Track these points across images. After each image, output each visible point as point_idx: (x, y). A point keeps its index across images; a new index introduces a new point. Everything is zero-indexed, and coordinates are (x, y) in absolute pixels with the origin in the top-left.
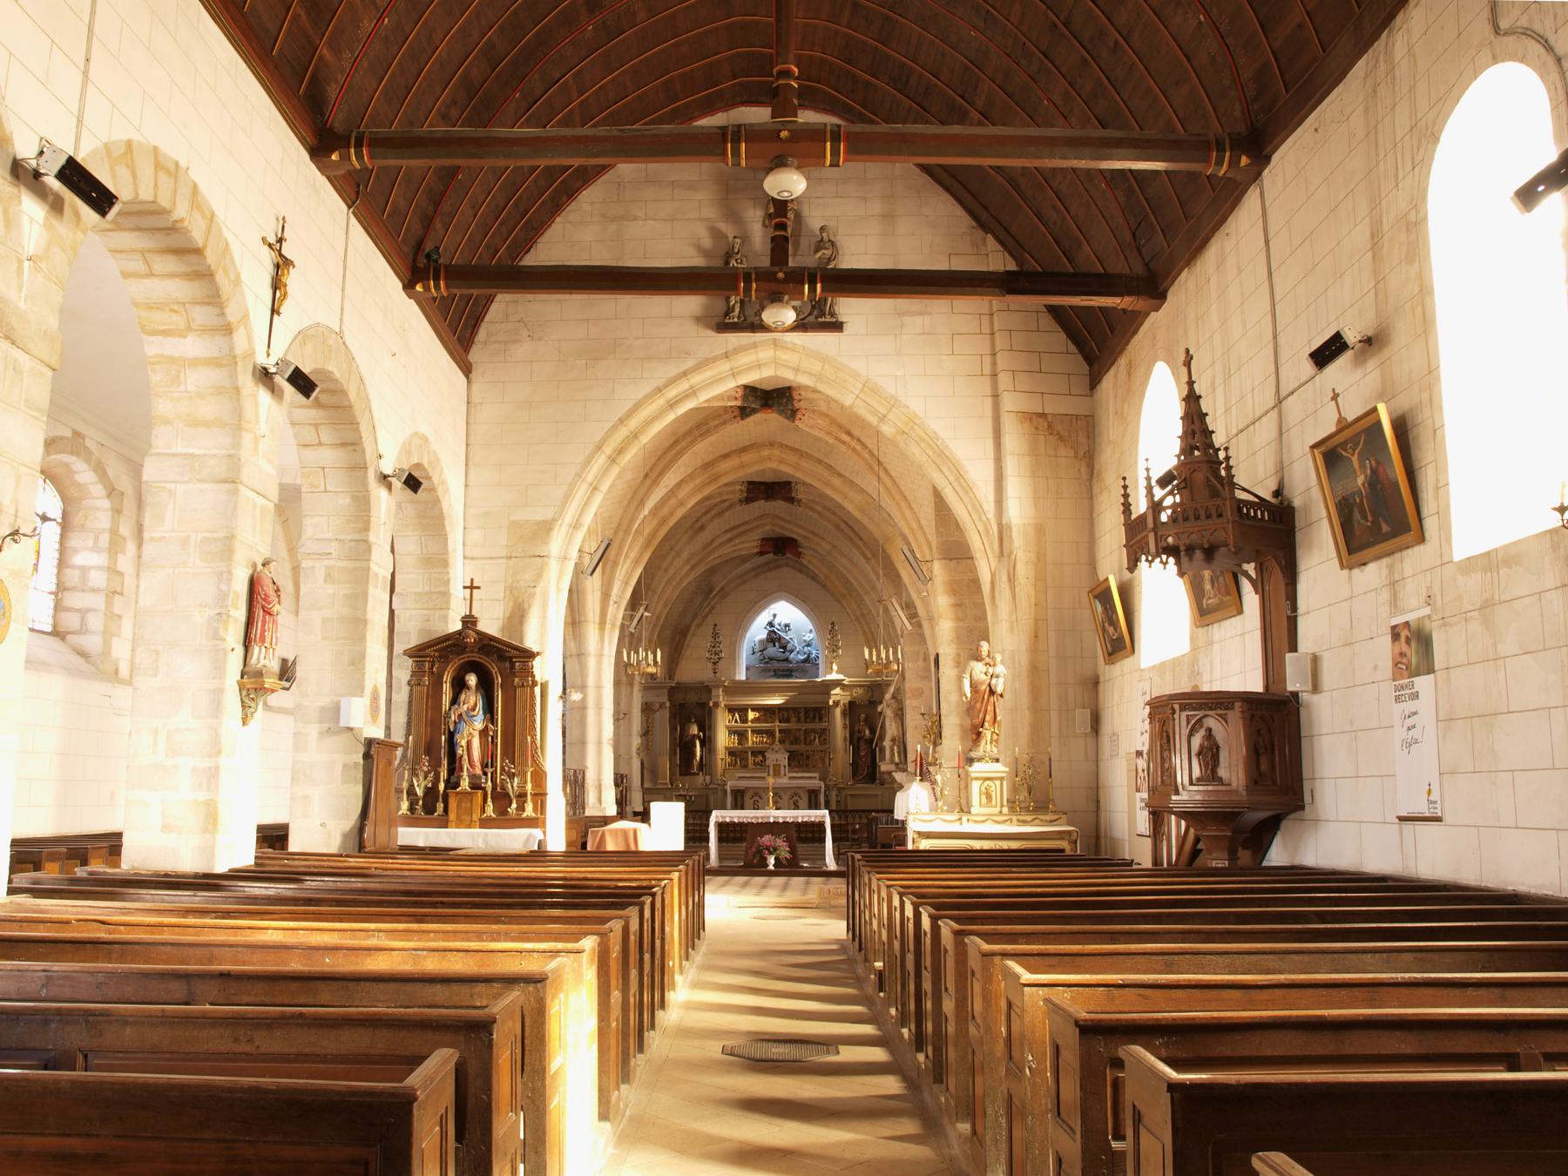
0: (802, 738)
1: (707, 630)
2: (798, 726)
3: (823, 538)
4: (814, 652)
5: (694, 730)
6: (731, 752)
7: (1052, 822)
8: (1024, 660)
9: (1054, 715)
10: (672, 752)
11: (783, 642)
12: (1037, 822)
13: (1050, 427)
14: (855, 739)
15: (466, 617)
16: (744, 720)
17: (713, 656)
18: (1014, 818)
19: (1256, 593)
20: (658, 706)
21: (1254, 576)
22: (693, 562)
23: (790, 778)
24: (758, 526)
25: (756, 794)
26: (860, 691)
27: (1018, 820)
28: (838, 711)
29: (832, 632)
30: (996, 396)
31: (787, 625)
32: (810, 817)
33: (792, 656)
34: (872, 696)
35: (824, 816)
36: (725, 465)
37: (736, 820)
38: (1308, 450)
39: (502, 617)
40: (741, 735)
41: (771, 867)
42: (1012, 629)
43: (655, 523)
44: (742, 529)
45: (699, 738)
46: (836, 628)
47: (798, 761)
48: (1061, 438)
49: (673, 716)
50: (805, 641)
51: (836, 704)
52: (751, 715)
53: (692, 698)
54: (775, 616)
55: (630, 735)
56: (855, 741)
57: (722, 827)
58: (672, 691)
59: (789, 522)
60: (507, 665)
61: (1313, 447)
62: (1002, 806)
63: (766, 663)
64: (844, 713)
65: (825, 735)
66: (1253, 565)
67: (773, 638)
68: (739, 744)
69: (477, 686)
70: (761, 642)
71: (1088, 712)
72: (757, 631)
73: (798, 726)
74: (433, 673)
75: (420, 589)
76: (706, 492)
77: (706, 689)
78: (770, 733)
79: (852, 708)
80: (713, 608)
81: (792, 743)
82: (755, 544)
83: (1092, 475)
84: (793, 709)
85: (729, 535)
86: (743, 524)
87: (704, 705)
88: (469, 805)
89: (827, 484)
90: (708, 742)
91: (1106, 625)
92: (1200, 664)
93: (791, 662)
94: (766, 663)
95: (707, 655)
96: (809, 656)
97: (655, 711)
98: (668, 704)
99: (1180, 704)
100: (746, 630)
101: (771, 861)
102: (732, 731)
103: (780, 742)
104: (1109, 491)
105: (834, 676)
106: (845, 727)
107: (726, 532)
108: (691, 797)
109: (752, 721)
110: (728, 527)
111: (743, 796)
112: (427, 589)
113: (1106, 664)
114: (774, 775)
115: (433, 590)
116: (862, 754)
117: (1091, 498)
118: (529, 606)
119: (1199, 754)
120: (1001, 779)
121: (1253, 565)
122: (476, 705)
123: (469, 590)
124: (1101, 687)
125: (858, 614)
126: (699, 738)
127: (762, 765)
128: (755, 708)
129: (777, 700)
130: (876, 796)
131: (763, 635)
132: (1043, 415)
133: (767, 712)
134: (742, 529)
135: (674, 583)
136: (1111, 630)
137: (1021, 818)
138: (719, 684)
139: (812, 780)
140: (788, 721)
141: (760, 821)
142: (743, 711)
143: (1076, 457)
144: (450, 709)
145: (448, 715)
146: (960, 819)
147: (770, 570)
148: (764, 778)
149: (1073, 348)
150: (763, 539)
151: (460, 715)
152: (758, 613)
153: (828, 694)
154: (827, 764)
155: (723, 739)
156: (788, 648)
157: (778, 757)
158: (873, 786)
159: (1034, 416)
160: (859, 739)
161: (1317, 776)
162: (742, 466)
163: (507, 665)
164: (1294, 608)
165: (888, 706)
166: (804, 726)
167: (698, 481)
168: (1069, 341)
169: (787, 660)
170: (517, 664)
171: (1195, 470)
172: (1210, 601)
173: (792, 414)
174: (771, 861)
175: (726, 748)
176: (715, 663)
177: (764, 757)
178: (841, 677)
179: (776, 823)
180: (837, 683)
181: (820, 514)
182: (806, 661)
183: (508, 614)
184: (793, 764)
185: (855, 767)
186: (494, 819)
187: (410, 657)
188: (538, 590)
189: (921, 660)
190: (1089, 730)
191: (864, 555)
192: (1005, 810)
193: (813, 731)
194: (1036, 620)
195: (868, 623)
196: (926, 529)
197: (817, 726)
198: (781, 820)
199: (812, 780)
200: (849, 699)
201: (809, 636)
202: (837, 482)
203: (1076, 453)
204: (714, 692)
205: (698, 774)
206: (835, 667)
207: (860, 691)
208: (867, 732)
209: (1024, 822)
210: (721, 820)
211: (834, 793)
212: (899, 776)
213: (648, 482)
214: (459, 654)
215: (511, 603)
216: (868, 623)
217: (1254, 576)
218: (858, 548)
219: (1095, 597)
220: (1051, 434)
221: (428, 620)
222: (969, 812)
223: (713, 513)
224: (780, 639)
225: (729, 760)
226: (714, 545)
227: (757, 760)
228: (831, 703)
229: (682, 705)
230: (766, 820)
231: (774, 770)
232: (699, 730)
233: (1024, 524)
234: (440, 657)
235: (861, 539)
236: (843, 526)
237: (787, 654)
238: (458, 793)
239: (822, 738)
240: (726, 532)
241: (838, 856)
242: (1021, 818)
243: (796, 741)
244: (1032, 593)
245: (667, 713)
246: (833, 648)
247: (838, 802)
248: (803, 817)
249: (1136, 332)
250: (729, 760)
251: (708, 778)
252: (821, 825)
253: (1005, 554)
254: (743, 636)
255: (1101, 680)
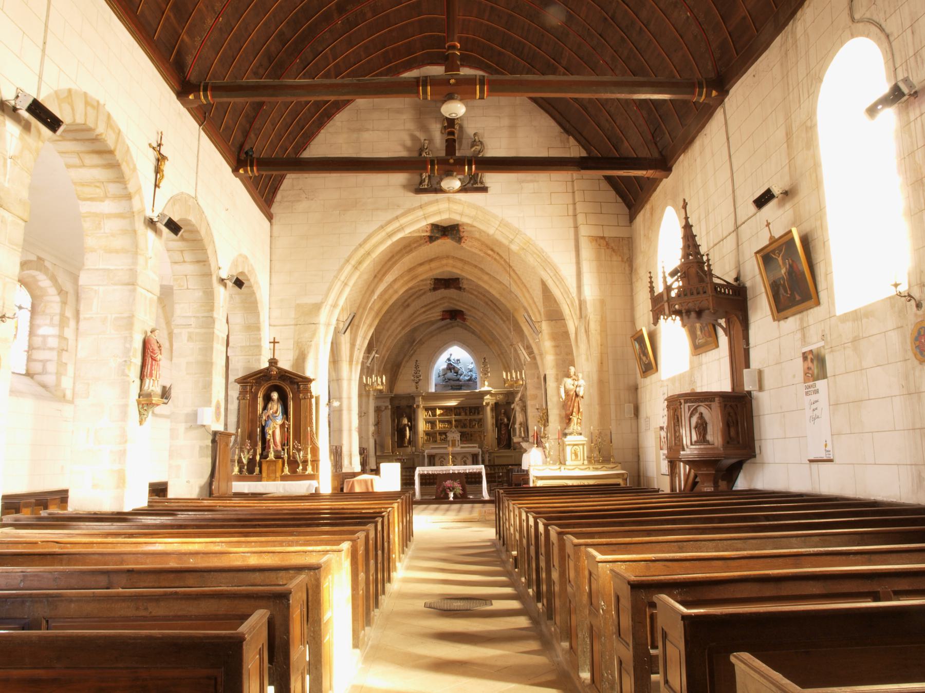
0: (468, 424)
1: (412, 363)
2: (466, 417)
3: (478, 310)
4: (474, 375)
5: (405, 421)
6: (427, 434)
7: (612, 468)
8: (595, 377)
9: (613, 408)
10: (393, 435)
11: (456, 369)
12: (604, 468)
13: (607, 244)
14: (498, 424)
15: (271, 359)
16: (434, 415)
17: (416, 379)
18: (591, 467)
19: (726, 335)
20: (384, 408)
21: (725, 326)
22: (403, 325)
23: (462, 447)
24: (441, 304)
25: (442, 457)
26: (501, 397)
27: (593, 468)
28: (488, 408)
29: (485, 363)
30: (576, 228)
31: (458, 360)
32: (473, 469)
33: (461, 377)
34: (508, 400)
35: (481, 469)
36: (421, 270)
37: (430, 473)
38: (754, 255)
39: (292, 359)
40: (433, 423)
41: (451, 499)
42: (587, 359)
43: (381, 303)
44: (431, 306)
45: (408, 425)
46: (487, 361)
47: (466, 437)
48: (613, 250)
49: (393, 413)
50: (469, 369)
51: (488, 404)
52: (438, 412)
53: (404, 403)
54: (451, 355)
55: (368, 425)
56: (499, 425)
57: (423, 477)
58: (392, 400)
59: (458, 301)
60: (296, 386)
61: (757, 253)
62: (584, 460)
63: (447, 382)
64: (492, 410)
65: (481, 422)
66: (724, 320)
67: (450, 368)
68: (431, 429)
69: (278, 399)
70: (443, 370)
71: (632, 406)
72: (441, 363)
73: (466, 417)
74: (252, 392)
75: (244, 344)
76: (410, 285)
77: (412, 398)
78: (449, 422)
79: (496, 407)
80: (415, 351)
81: (462, 427)
82: (439, 314)
83: (632, 271)
84: (463, 408)
85: (424, 310)
86: (432, 303)
87: (411, 407)
88: (274, 468)
89: (480, 279)
90: (413, 428)
91: (641, 355)
92: (695, 376)
93: (461, 381)
94: (447, 382)
95: (412, 378)
96: (471, 377)
97: (382, 411)
98: (390, 407)
99: (685, 400)
100: (434, 363)
101: (451, 495)
102: (427, 422)
103: (455, 427)
104: (642, 280)
105: (486, 388)
106: (493, 418)
107: (422, 307)
108: (404, 460)
109: (439, 415)
110: (423, 305)
111: (434, 459)
112: (248, 344)
113: (642, 378)
114: (452, 446)
115: (252, 344)
116: (503, 432)
117: (631, 284)
118: (308, 352)
119: (696, 427)
120: (583, 445)
121: (724, 320)
122: (277, 410)
123: (272, 344)
124: (639, 390)
125: (499, 353)
126: (408, 425)
127: (445, 440)
128: (440, 408)
129: (453, 403)
130: (511, 456)
131: (445, 366)
132: (603, 238)
133: (447, 410)
134: (431, 306)
135: (392, 338)
136: (644, 358)
137: (594, 466)
138: (419, 395)
139: (474, 448)
140: (460, 414)
141: (444, 472)
142: (433, 409)
143: (622, 261)
144: (262, 413)
145: (261, 416)
146: (560, 468)
147: (448, 328)
148: (446, 448)
149: (619, 200)
150: (443, 311)
151: (268, 416)
152: (441, 353)
153: (482, 399)
154: (483, 439)
155: (422, 426)
156: (459, 373)
157: (455, 435)
158: (510, 450)
159: (598, 239)
160: (501, 424)
161: (763, 438)
162: (431, 269)
163: (296, 386)
164: (748, 344)
165: (517, 405)
166: (469, 418)
167: (405, 279)
168: (617, 196)
169: (458, 380)
170: (301, 386)
171: (690, 267)
172: (700, 341)
173: (459, 240)
174: (451, 495)
175: (424, 431)
176: (417, 383)
177: (446, 436)
178: (490, 389)
179: (454, 474)
180: (488, 393)
181: (476, 296)
182: (469, 380)
183: (295, 357)
184: (463, 439)
185: (499, 440)
186: (289, 476)
187: (239, 383)
188: (313, 343)
189: (536, 377)
190: (633, 415)
191: (502, 319)
192: (586, 462)
193: (475, 420)
194: (601, 354)
195: (504, 358)
196: (537, 304)
197: (476, 417)
198: (456, 472)
199: (474, 448)
200: (494, 401)
201: (471, 366)
202: (486, 278)
203: (622, 259)
204: (416, 399)
205: (407, 447)
206: (486, 383)
207: (501, 397)
208: (506, 420)
209: (597, 469)
210: (421, 472)
211: (487, 456)
212: (524, 445)
213: (376, 280)
214: (267, 381)
215: (297, 351)
216: (504, 358)
217: (725, 326)
218: (499, 315)
219: (635, 340)
220: (608, 248)
221: (249, 362)
222: (565, 464)
223: (414, 297)
224: (454, 368)
225: (426, 438)
226: (415, 315)
227: (442, 438)
228: (484, 404)
229: (398, 407)
230: (448, 472)
231: (452, 444)
232: (408, 421)
233: (594, 299)
234: (256, 383)
235: (500, 310)
236: (490, 303)
237: (459, 376)
238: (267, 461)
239: (480, 424)
240: (422, 307)
241: (490, 491)
242: (594, 466)
243: (464, 426)
244: (599, 338)
245: (389, 412)
246: (485, 373)
247: (489, 460)
248: (469, 470)
249: (655, 190)
250: (426, 438)
251: (414, 449)
252: (479, 475)
253: (583, 317)
254: (432, 367)
255: (639, 387)
